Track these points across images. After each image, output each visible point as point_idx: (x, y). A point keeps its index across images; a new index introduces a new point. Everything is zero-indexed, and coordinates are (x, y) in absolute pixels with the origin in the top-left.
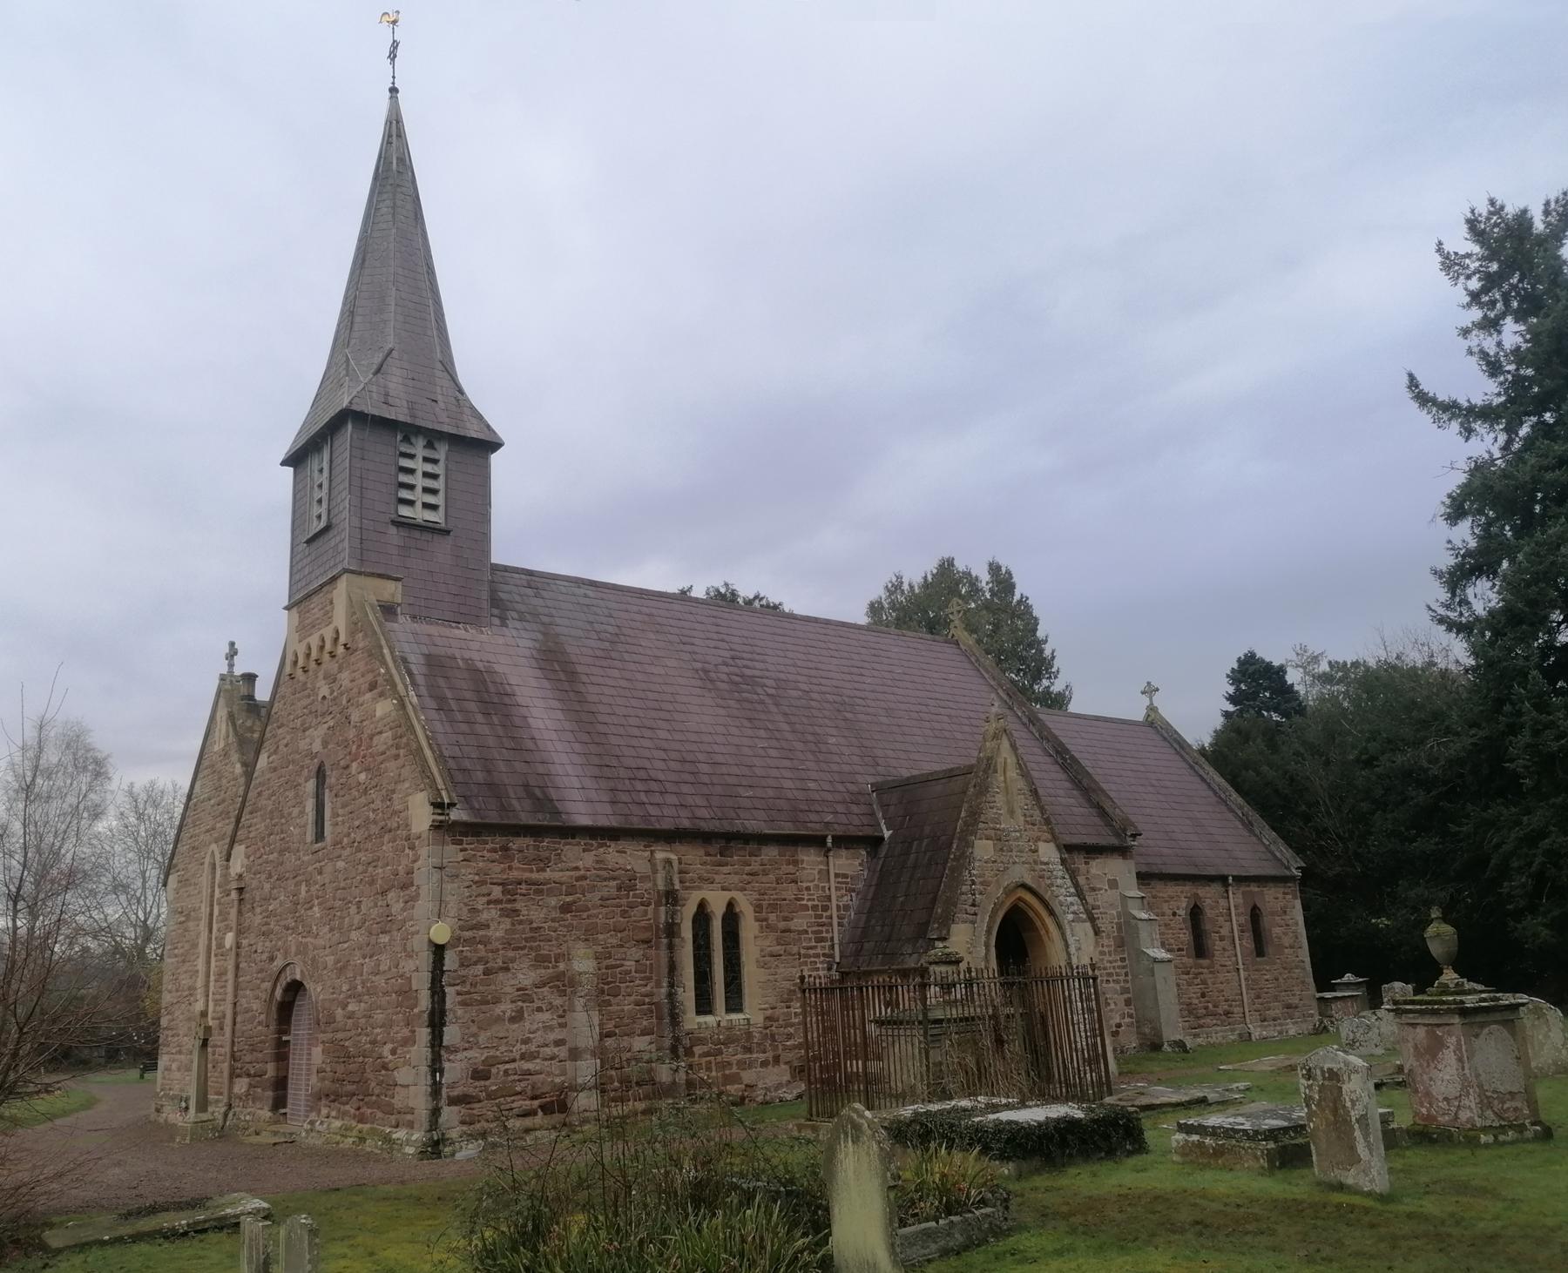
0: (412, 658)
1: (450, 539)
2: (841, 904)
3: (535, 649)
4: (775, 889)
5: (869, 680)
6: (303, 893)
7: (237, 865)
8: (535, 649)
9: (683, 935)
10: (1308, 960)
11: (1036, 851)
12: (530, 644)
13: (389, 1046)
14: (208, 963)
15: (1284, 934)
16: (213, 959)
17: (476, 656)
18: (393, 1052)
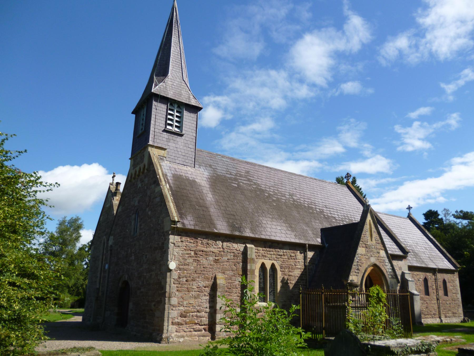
0: (168, 174)
1: (183, 137)
2: (310, 268)
3: (209, 178)
4: (287, 261)
5: (320, 196)
6: (129, 251)
7: (110, 243)
8: (209, 178)
9: (255, 274)
10: (460, 298)
11: (379, 253)
12: (208, 174)
13: (154, 303)
14: (101, 274)
15: (453, 289)
16: (102, 273)
17: (190, 176)
18: (155, 305)
